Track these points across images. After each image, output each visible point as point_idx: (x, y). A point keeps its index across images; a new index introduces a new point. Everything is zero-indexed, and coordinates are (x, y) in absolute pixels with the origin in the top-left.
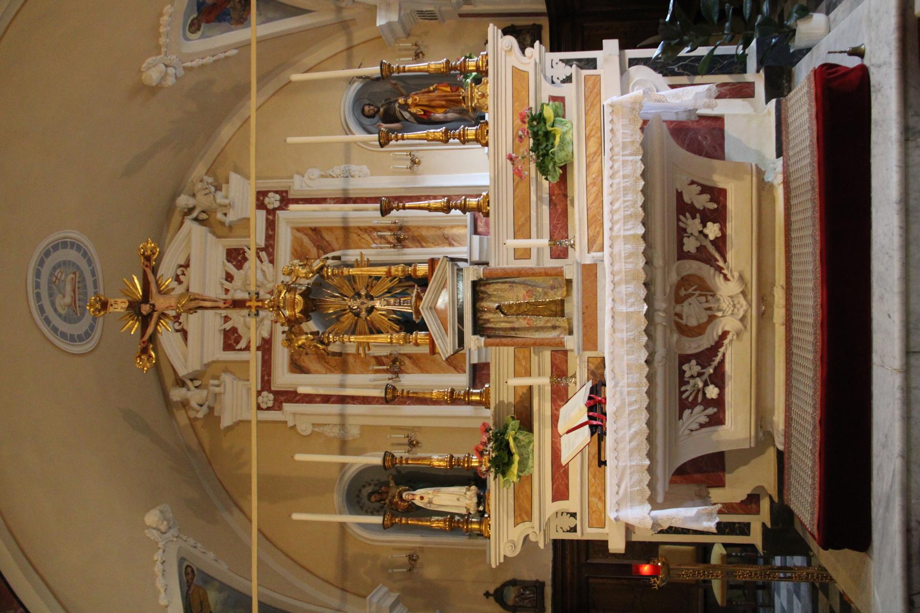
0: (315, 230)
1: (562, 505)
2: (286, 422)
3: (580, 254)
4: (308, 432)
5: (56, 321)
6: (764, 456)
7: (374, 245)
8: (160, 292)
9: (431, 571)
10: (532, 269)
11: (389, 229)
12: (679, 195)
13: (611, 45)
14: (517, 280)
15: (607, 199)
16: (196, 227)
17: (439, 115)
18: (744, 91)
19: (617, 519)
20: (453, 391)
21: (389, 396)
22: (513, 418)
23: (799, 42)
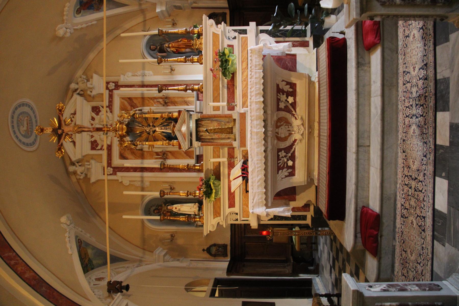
0: (130, 99)
1: (232, 210)
2: (118, 180)
3: (239, 109)
4: (128, 184)
5: (21, 137)
6: (311, 189)
7: (155, 105)
8: (66, 125)
9: (180, 241)
10: (220, 115)
11: (161, 98)
12: (278, 85)
13: (253, 24)
14: (214, 119)
15: (249, 87)
17: (183, 50)
18: (305, 44)
19: (253, 213)
20: (188, 165)
21: (162, 167)
22: (213, 175)
23: (325, 26)
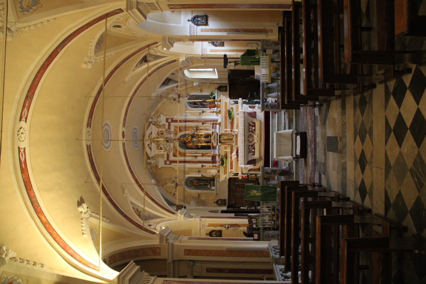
1: (232, 170)
11: (195, 127)
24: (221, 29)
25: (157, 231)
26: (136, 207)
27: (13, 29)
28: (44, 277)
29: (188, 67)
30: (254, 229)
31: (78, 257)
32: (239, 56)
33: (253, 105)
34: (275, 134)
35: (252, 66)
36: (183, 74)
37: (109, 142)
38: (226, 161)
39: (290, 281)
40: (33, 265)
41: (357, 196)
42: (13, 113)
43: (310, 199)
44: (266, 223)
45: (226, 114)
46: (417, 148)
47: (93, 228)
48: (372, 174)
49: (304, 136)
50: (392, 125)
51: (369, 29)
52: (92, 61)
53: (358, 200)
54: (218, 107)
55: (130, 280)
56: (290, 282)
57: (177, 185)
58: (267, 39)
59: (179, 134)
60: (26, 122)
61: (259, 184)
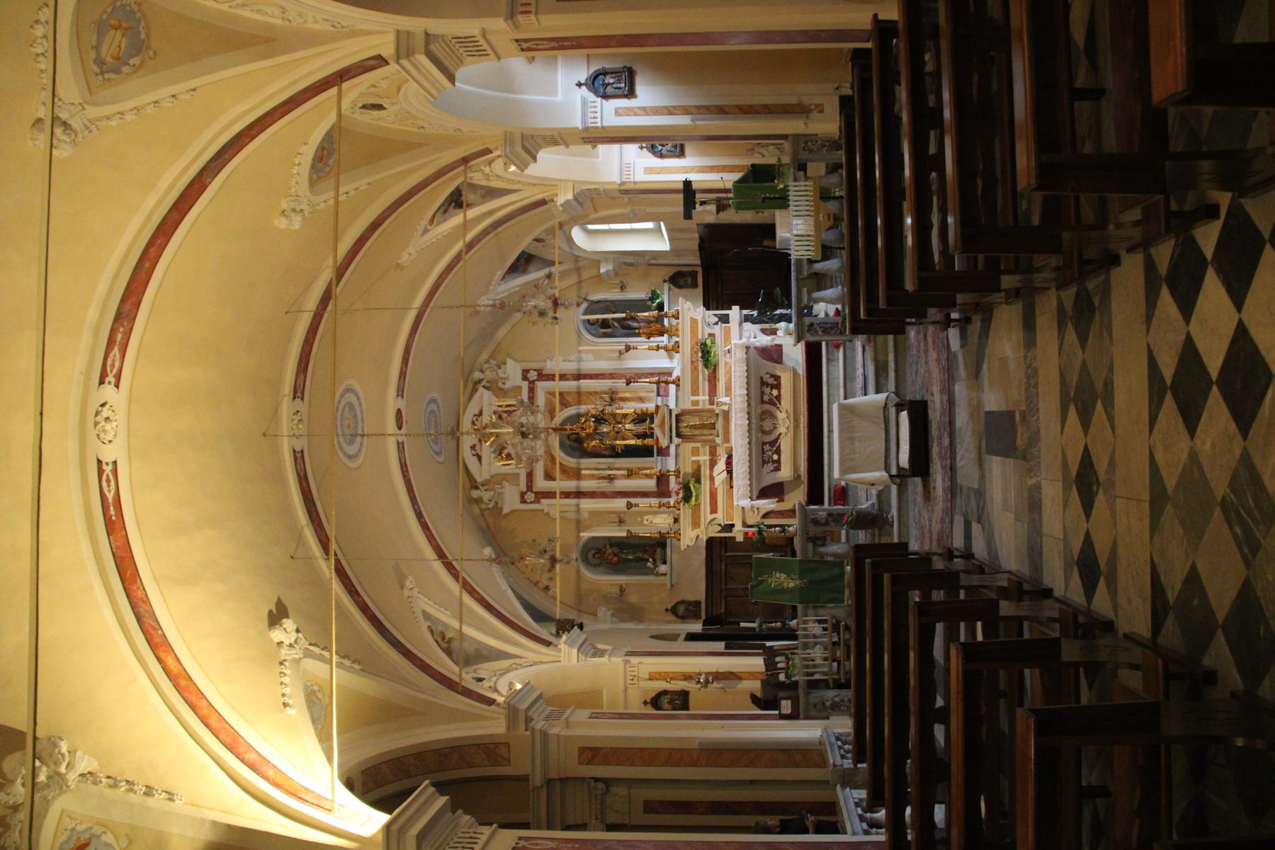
9: (633, 598)
16: (485, 391)
24: (674, 107)
25: (500, 694)
26: (440, 628)
27: (74, 123)
28: (174, 829)
29: (582, 221)
30: (782, 685)
31: (271, 773)
32: (729, 185)
33: (774, 326)
34: (835, 407)
35: (767, 213)
36: (570, 241)
37: (359, 439)
38: (696, 490)
39: (881, 837)
40: (145, 794)
41: (1072, 584)
42: (80, 362)
43: (938, 595)
44: (815, 666)
45: (694, 353)
46: (1239, 437)
47: (316, 688)
48: (1114, 516)
49: (919, 412)
50: (1168, 372)
51: (1096, 94)
52: (302, 207)
53: (1076, 595)
54: (671, 332)
55: (421, 837)
56: (882, 838)
57: (553, 560)
58: (808, 131)
59: (561, 415)
60: (117, 386)
61: (794, 554)
